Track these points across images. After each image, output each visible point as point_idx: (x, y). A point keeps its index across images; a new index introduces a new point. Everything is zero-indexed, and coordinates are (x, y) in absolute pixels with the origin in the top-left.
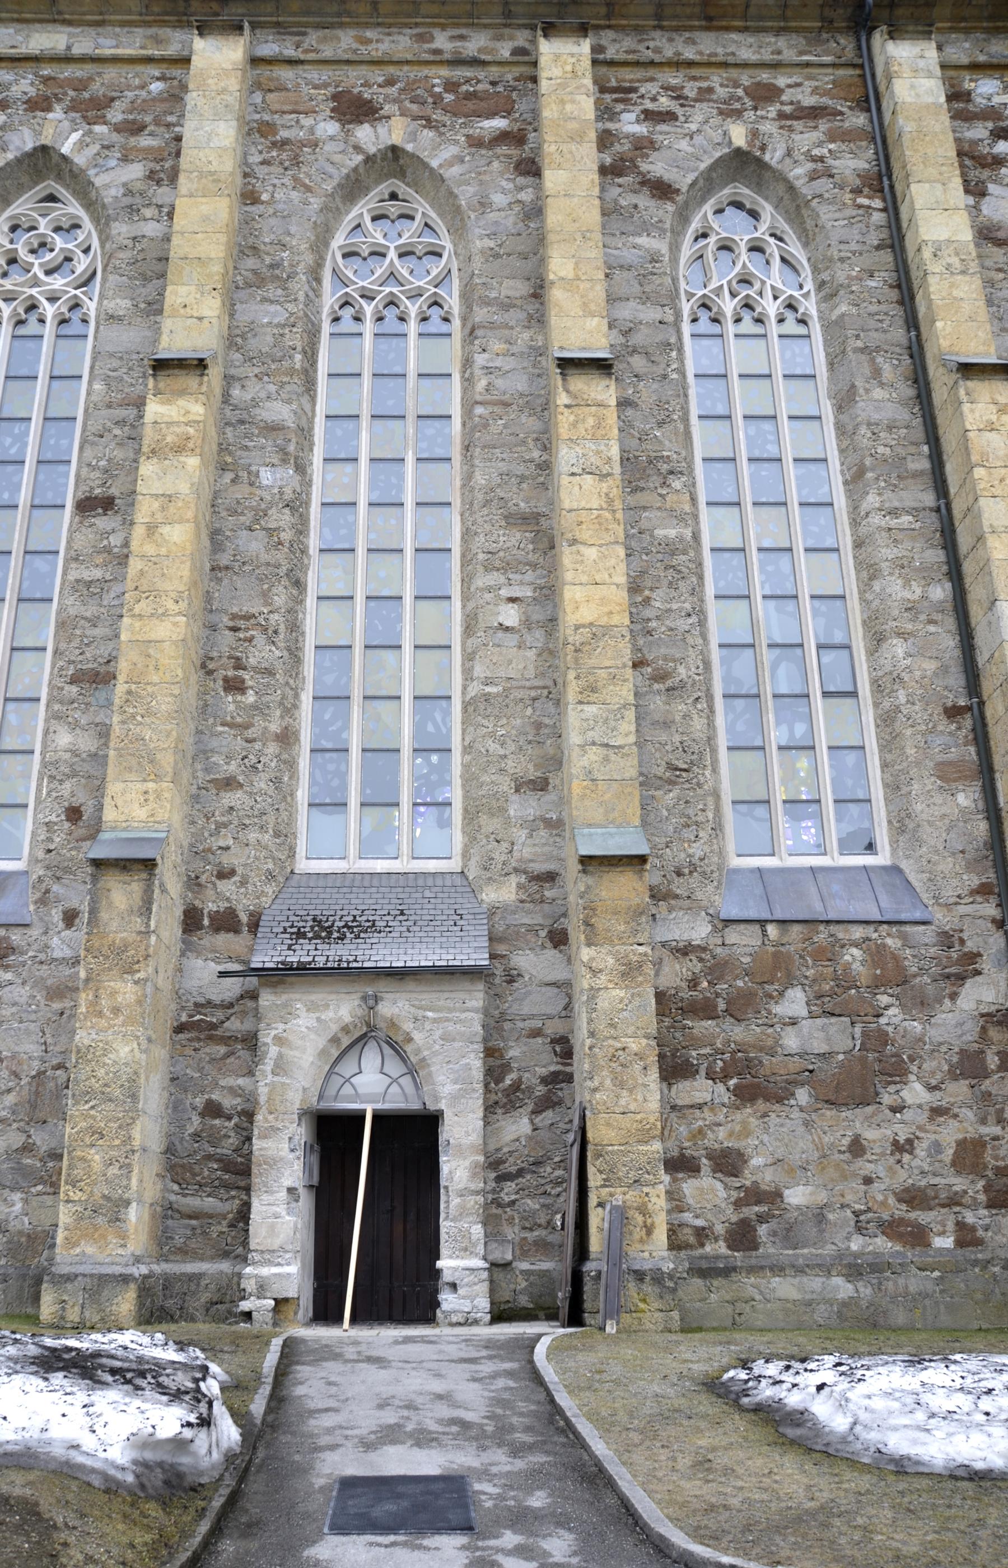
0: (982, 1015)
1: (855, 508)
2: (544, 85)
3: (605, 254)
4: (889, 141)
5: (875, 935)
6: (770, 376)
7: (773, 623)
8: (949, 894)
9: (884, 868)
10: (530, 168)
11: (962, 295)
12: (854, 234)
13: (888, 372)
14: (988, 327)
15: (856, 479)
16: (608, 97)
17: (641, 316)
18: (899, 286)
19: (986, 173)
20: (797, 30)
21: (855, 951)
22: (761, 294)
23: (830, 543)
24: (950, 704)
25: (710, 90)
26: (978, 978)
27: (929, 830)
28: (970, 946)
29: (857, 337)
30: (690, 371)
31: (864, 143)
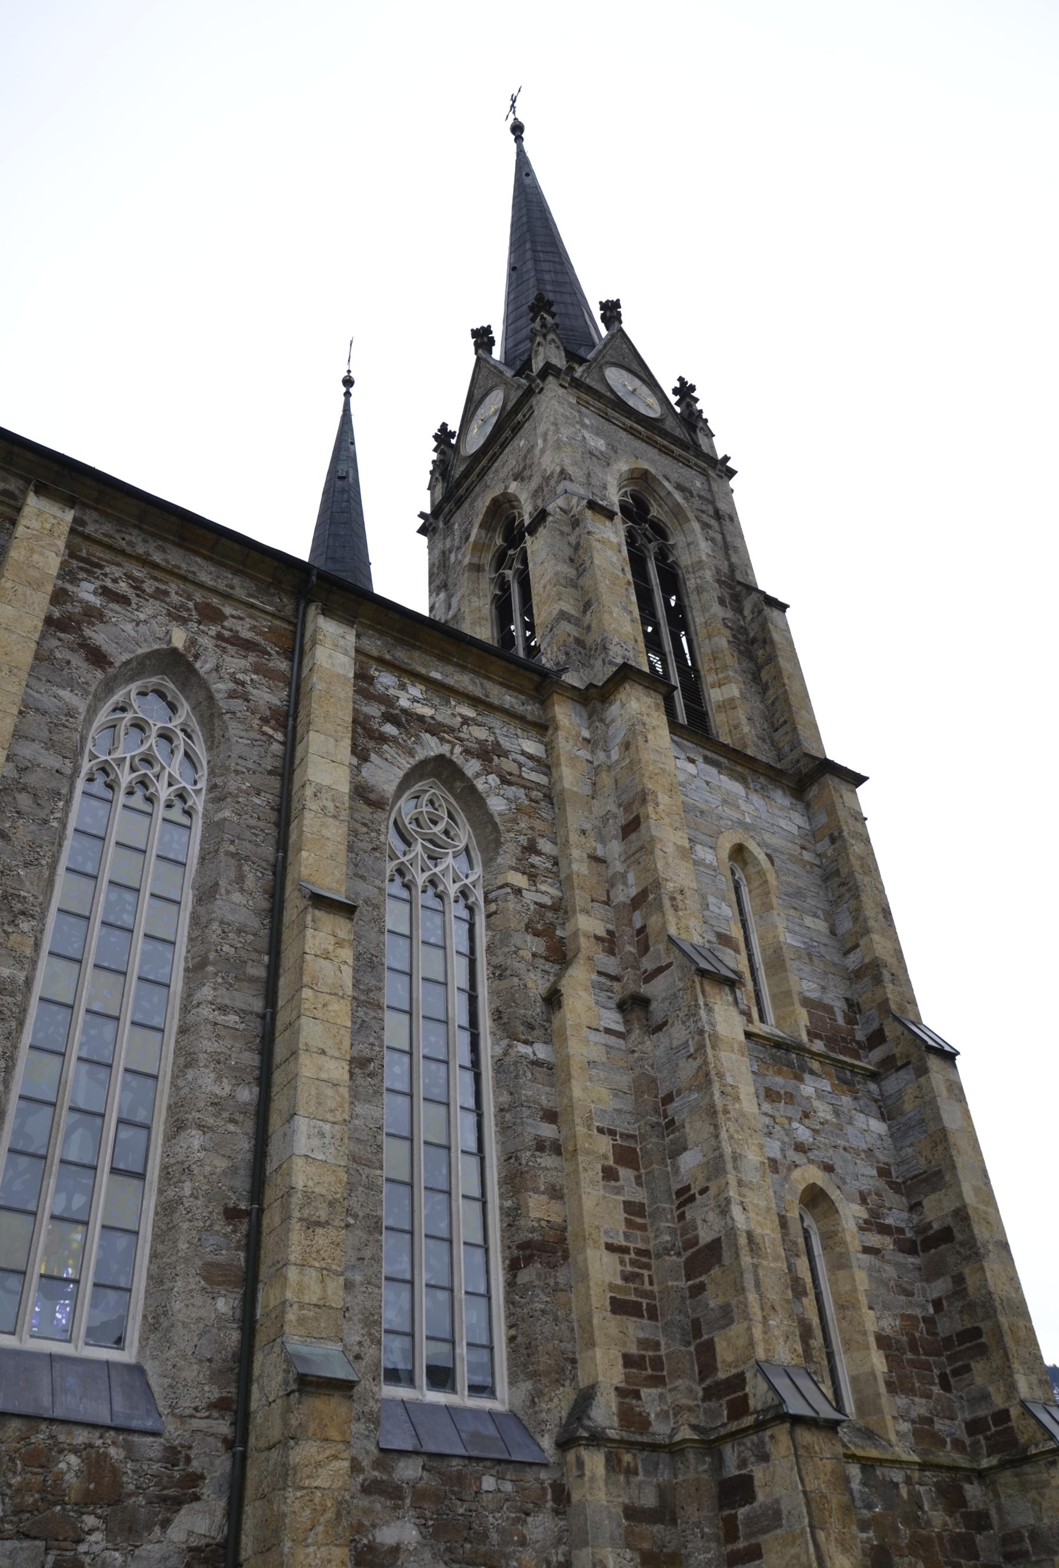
0: (190, 1549)
1: (189, 996)
2: (20, 531)
3: (25, 693)
4: (302, 691)
5: (99, 1442)
6: (144, 852)
7: (79, 1085)
8: (186, 1404)
9: (127, 1367)
11: (329, 835)
12: (254, 754)
13: (250, 881)
14: (344, 869)
15: (196, 969)
16: (75, 563)
17: (41, 760)
18: (279, 811)
19: (371, 744)
20: (252, 577)
21: (73, 1459)
22: (158, 777)
23: (156, 1022)
24: (231, 1205)
26: (196, 1505)
27: (182, 1331)
28: (196, 1465)
29: (232, 842)
30: (72, 823)
31: (281, 684)
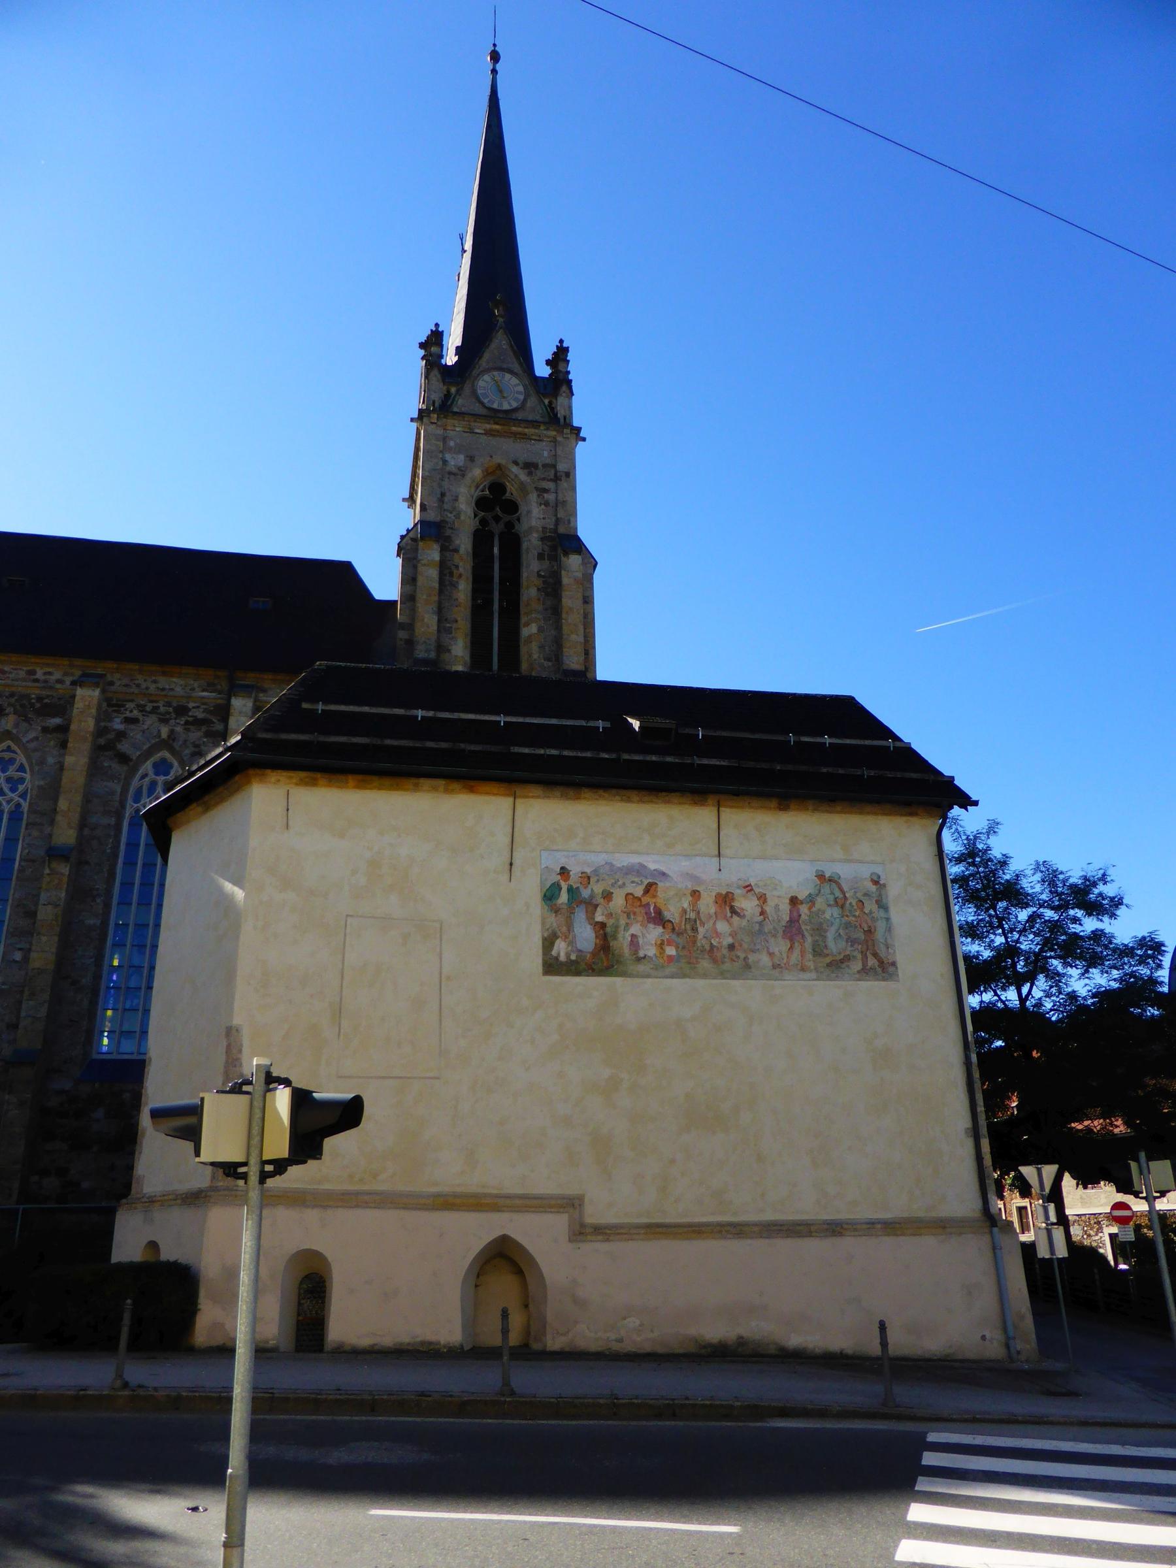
10: (64, 745)
25: (158, 707)
